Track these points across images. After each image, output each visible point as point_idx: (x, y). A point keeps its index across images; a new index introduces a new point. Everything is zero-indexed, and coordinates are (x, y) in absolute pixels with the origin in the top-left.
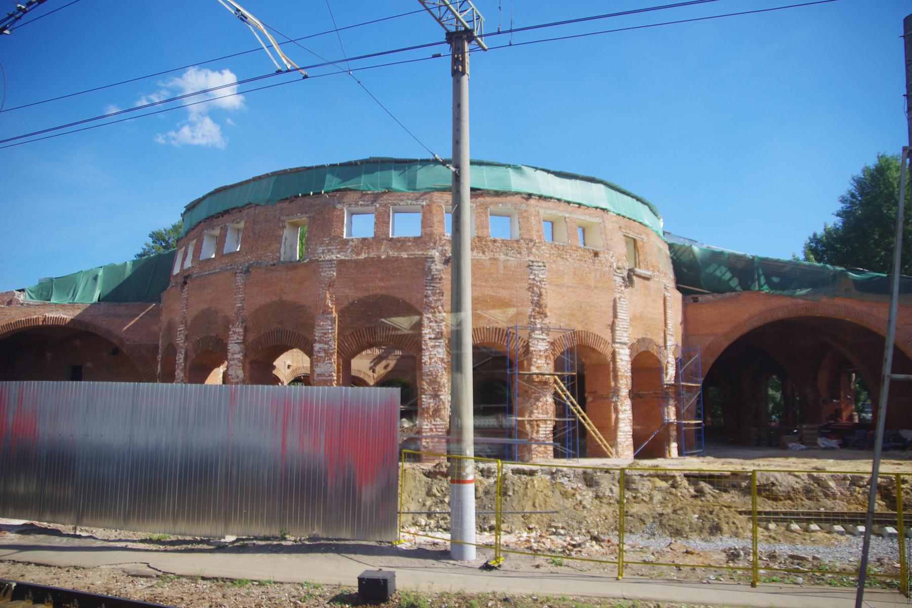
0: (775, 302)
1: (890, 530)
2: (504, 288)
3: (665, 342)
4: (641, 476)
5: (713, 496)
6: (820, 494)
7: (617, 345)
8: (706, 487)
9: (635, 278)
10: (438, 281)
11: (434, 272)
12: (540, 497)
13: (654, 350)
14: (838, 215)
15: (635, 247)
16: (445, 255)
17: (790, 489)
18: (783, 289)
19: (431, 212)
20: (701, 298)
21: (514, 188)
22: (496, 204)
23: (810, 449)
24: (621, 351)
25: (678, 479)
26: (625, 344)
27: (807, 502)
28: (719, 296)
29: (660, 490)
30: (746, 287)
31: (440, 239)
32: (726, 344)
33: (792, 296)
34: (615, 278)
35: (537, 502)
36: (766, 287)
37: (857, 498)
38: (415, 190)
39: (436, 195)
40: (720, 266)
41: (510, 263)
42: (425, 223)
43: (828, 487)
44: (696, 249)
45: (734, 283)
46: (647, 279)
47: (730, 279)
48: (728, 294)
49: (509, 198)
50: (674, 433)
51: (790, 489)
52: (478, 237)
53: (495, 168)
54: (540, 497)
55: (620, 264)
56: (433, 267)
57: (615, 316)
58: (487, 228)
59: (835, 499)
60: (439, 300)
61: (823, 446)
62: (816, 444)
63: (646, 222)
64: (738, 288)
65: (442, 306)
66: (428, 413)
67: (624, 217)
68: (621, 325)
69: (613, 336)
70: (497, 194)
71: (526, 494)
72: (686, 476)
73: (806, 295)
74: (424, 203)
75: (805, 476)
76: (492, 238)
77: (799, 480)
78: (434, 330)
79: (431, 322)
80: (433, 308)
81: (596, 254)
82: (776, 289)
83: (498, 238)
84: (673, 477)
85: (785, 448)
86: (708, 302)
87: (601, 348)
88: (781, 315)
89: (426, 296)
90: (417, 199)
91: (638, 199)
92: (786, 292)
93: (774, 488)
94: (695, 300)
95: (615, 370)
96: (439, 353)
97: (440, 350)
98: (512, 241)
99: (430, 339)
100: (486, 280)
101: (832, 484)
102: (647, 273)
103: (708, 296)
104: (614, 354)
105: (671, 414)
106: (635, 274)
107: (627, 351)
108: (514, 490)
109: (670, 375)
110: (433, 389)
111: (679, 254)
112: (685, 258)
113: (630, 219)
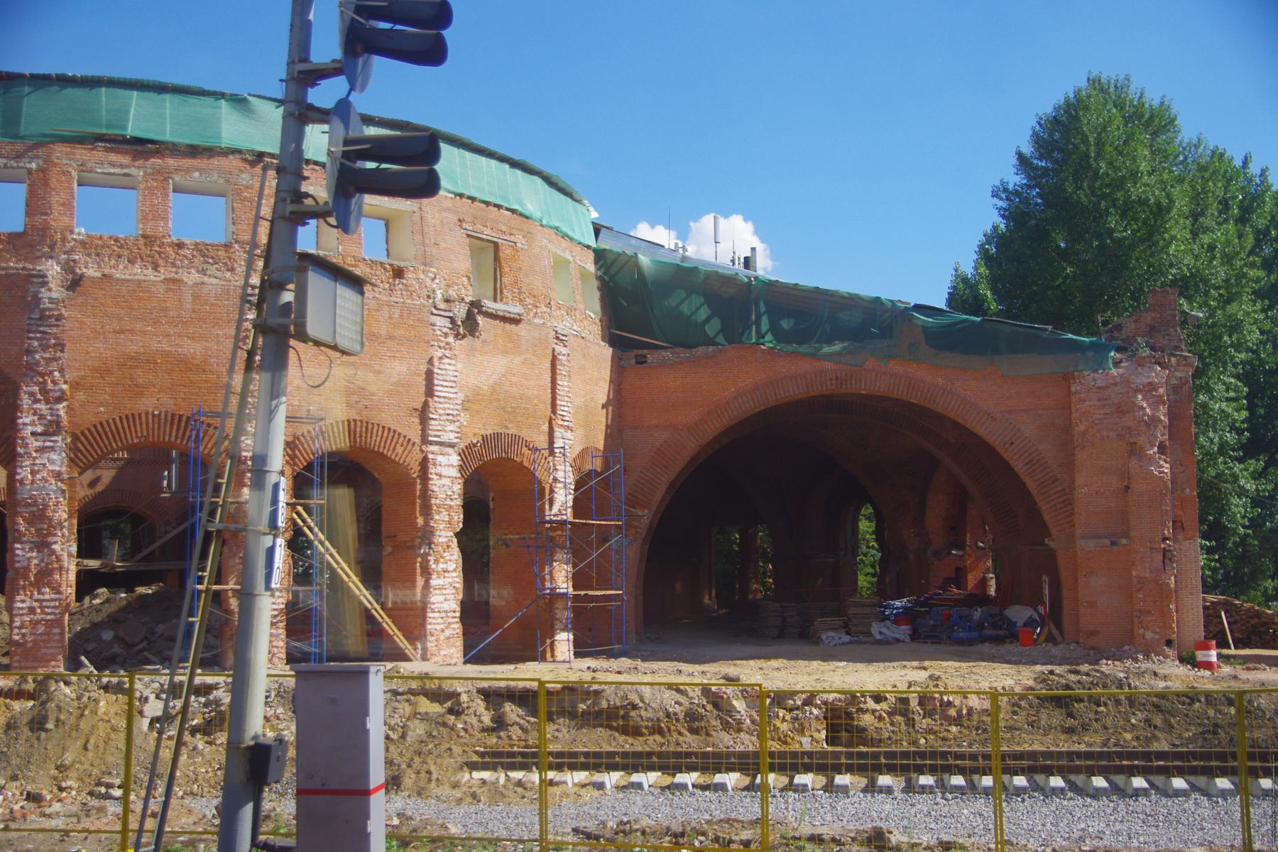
1: (1223, 783)
2: (193, 338)
5: (522, 728)
6: (716, 723)
7: (432, 448)
8: (512, 711)
9: (480, 319)
10: (53, 321)
11: (46, 304)
12: (102, 729)
13: (526, 457)
14: (1263, 173)
15: (497, 258)
16: (72, 271)
18: (800, 343)
19: (46, 184)
20: (651, 357)
21: (227, 140)
22: (188, 171)
24: (440, 458)
25: (464, 698)
26: (452, 446)
27: (689, 737)
28: (685, 354)
29: (425, 717)
31: (64, 239)
32: (691, 446)
33: (815, 356)
35: (92, 741)
36: (769, 337)
37: (776, 729)
38: (16, 136)
39: (59, 150)
40: (688, 296)
41: (206, 289)
42: (35, 206)
43: (731, 711)
44: (644, 260)
45: (713, 328)
46: (516, 321)
47: (708, 320)
48: (701, 350)
49: (215, 161)
50: (564, 614)
52: (144, 236)
53: (193, 100)
54: (102, 729)
55: (452, 293)
56: (44, 294)
57: (430, 392)
58: (165, 219)
59: (739, 730)
60: (55, 359)
61: (878, 637)
62: (869, 634)
63: (530, 208)
64: (720, 339)
65: (61, 371)
66: (26, 577)
67: (473, 199)
68: (439, 408)
69: (424, 430)
70: (194, 151)
71: (77, 728)
72: (480, 691)
73: (839, 353)
74: (34, 166)
75: (696, 693)
76: (174, 239)
77: (681, 699)
78: (42, 417)
79: (37, 401)
80: (42, 375)
81: (399, 273)
82: (788, 342)
83: (188, 241)
85: (818, 641)
87: (398, 453)
88: (793, 391)
89: (29, 352)
90: (19, 157)
91: (514, 164)
92: (804, 349)
93: (633, 713)
94: (641, 361)
95: (426, 495)
96: (52, 462)
97: (54, 456)
98: (216, 247)
99: (33, 434)
100: (156, 322)
101: (739, 705)
102: (514, 309)
105: (561, 577)
106: (480, 312)
107: (455, 459)
108: (58, 720)
109: (562, 503)
110: (39, 531)
111: (613, 271)
113: (487, 203)
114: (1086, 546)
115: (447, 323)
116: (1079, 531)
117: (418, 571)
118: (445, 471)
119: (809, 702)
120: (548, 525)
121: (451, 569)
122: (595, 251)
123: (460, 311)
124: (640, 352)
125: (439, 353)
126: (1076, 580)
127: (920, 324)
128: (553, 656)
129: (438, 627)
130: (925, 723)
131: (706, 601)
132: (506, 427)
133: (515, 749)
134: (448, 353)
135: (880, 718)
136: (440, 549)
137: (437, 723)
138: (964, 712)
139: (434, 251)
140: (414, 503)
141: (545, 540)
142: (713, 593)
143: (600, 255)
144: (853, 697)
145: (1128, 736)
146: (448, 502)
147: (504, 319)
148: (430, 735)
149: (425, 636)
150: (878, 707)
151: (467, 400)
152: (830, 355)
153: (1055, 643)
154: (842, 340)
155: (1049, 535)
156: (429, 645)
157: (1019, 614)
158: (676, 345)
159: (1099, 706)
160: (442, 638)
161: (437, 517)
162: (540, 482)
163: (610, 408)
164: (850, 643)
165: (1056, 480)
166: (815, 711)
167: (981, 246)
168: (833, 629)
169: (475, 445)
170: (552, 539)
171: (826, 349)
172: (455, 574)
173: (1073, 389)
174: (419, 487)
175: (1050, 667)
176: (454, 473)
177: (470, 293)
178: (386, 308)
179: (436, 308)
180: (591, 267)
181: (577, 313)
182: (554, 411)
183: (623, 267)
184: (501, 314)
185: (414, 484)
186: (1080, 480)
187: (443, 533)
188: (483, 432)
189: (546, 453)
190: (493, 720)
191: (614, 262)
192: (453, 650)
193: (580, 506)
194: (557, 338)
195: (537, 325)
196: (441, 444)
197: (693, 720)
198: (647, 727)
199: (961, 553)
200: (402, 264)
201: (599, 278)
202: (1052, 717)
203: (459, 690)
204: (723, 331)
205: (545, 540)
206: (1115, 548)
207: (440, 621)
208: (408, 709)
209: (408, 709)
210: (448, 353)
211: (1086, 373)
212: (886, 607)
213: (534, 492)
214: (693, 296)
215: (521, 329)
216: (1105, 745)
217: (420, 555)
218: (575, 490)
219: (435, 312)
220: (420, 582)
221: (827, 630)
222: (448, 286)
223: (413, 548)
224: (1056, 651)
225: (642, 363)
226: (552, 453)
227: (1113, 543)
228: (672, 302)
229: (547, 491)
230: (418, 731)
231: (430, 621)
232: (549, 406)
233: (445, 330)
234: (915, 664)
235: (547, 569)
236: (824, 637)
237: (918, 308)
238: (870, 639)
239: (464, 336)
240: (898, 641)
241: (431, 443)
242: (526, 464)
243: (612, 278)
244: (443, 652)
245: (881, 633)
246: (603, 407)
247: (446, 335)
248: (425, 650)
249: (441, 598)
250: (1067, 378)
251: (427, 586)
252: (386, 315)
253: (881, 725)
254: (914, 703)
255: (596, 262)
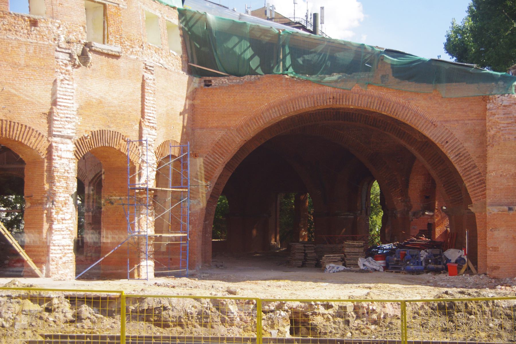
0: (301, 90)
3: (141, 137)
4: (9, 297)
7: (55, 139)
8: (86, 310)
9: (91, 55)
13: (123, 146)
15: (105, 14)
17: (182, 314)
18: (311, 74)
20: (215, 82)
23: (351, 271)
24: (60, 146)
25: (55, 301)
26: (70, 138)
28: (236, 80)
30: (268, 70)
32: (239, 141)
33: (319, 83)
34: (57, 54)
36: (291, 70)
45: (255, 63)
46: (116, 57)
47: (252, 57)
48: (247, 78)
51: (182, 314)
55: (72, 37)
57: (54, 103)
61: (362, 267)
62: (356, 265)
64: (259, 71)
69: (50, 127)
72: (66, 297)
73: (336, 81)
77: (197, 304)
81: (34, 23)
84: (49, 299)
86: (221, 87)
87: (31, 142)
88: (305, 106)
92: (313, 78)
93: (164, 313)
94: (208, 84)
95: (50, 170)
101: (233, 308)
102: (114, 48)
103: (223, 79)
104: (50, 149)
106: (91, 50)
107: (71, 147)
109: (147, 178)
111: (191, 24)
112: (198, 30)
114: (492, 210)
115: (67, 57)
116: (488, 201)
117: (45, 219)
118: (64, 155)
119: (280, 307)
120: (137, 191)
121: (67, 218)
122: (179, 10)
123: (77, 50)
124: (207, 78)
125: (61, 77)
126: (486, 232)
127: (389, 62)
128: (139, 275)
129: (58, 256)
130: (355, 323)
131: (273, 242)
132: (109, 127)
133: (84, 334)
134: (67, 77)
135: (328, 319)
136: (60, 205)
137: (36, 317)
138: (382, 316)
139: (59, 9)
140: (43, 175)
141: (136, 199)
142: (278, 237)
143: (182, 13)
144: (309, 304)
145: (483, 334)
146: (66, 174)
147: (108, 55)
148: (31, 325)
149: (49, 261)
150: (326, 312)
151: (81, 108)
152: (331, 82)
153: (471, 274)
154: (339, 73)
155: (471, 203)
156: (51, 267)
157: (453, 254)
158: (231, 74)
159: (471, 314)
160: (60, 262)
161: (58, 184)
162: (132, 163)
163: (186, 115)
164: (344, 271)
165: (475, 167)
166: (283, 313)
167: (470, 7)
168: (334, 262)
169: (86, 138)
170: (140, 200)
171: (328, 78)
172: (70, 222)
173: (488, 107)
174: (46, 164)
175: (446, 289)
176: (71, 155)
177: (85, 37)
178: (24, 47)
179: (59, 46)
180: (175, 21)
181: (164, 52)
182: (143, 116)
183: (197, 21)
184: (105, 52)
185: (43, 162)
186: (491, 166)
187: (62, 195)
188: (92, 129)
189: (137, 144)
190: (74, 316)
191: (191, 18)
192: (67, 271)
193: (160, 176)
194: (146, 68)
195: (134, 60)
196: (62, 137)
197: (203, 318)
198: (172, 322)
199: (431, 214)
200: (36, 17)
201: (181, 29)
202: (442, 321)
203: (52, 296)
204: (261, 65)
205: (136, 199)
206: (511, 212)
207: (59, 251)
208: (18, 308)
209: (18, 308)
210: (67, 77)
211: (497, 96)
212: (379, 248)
213: (127, 170)
214: (243, 42)
215: (120, 62)
216: (465, 339)
217: (47, 209)
218: (158, 167)
219: (58, 49)
220: (46, 226)
221: (330, 262)
222: (69, 32)
223: (42, 204)
224: (471, 279)
225: (208, 86)
226: (141, 144)
227: (510, 209)
228: (230, 44)
229: (137, 168)
230: (23, 322)
231: (51, 251)
232: (140, 113)
233: (65, 62)
234: (355, 285)
235: (136, 219)
236: (327, 266)
237: (389, 52)
238: (357, 269)
239: (79, 66)
240: (375, 270)
241: (55, 136)
242: (122, 150)
243: (190, 29)
244: (60, 272)
245: (364, 265)
246: (181, 114)
247: (66, 65)
248: (48, 271)
249: (60, 237)
250: (485, 99)
251: (50, 228)
252: (24, 50)
253: (328, 323)
254: (350, 310)
255: (179, 18)
